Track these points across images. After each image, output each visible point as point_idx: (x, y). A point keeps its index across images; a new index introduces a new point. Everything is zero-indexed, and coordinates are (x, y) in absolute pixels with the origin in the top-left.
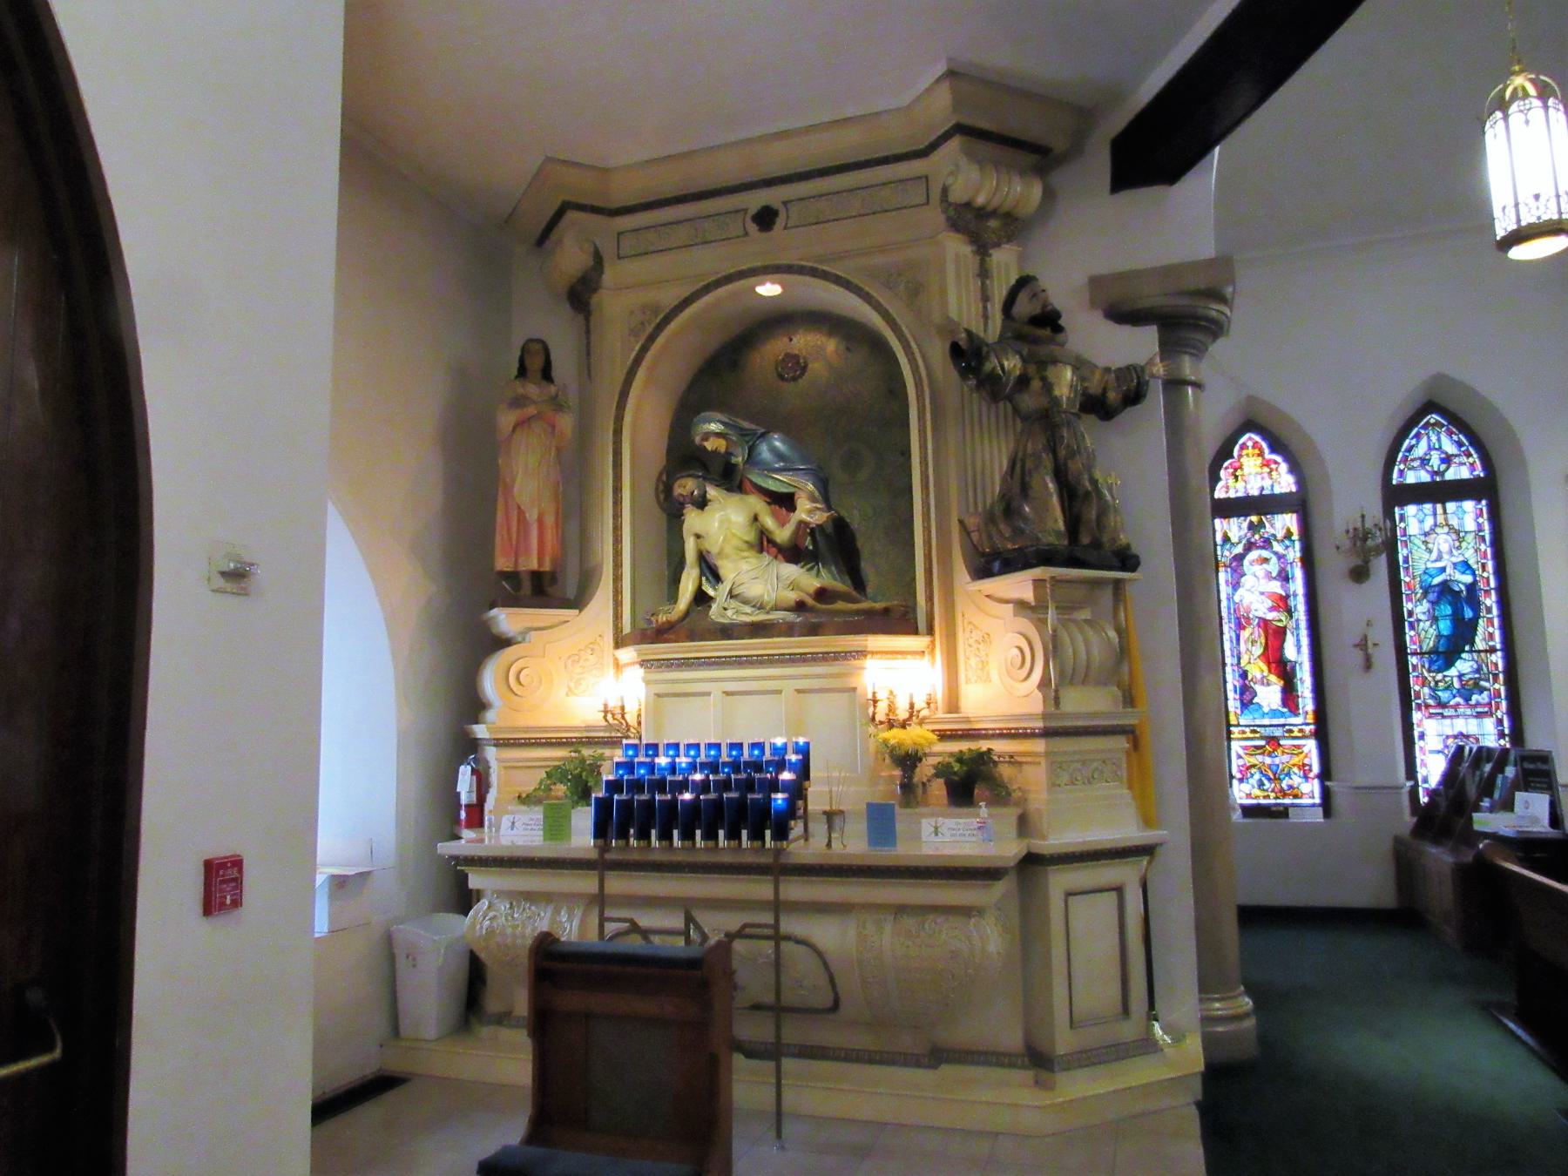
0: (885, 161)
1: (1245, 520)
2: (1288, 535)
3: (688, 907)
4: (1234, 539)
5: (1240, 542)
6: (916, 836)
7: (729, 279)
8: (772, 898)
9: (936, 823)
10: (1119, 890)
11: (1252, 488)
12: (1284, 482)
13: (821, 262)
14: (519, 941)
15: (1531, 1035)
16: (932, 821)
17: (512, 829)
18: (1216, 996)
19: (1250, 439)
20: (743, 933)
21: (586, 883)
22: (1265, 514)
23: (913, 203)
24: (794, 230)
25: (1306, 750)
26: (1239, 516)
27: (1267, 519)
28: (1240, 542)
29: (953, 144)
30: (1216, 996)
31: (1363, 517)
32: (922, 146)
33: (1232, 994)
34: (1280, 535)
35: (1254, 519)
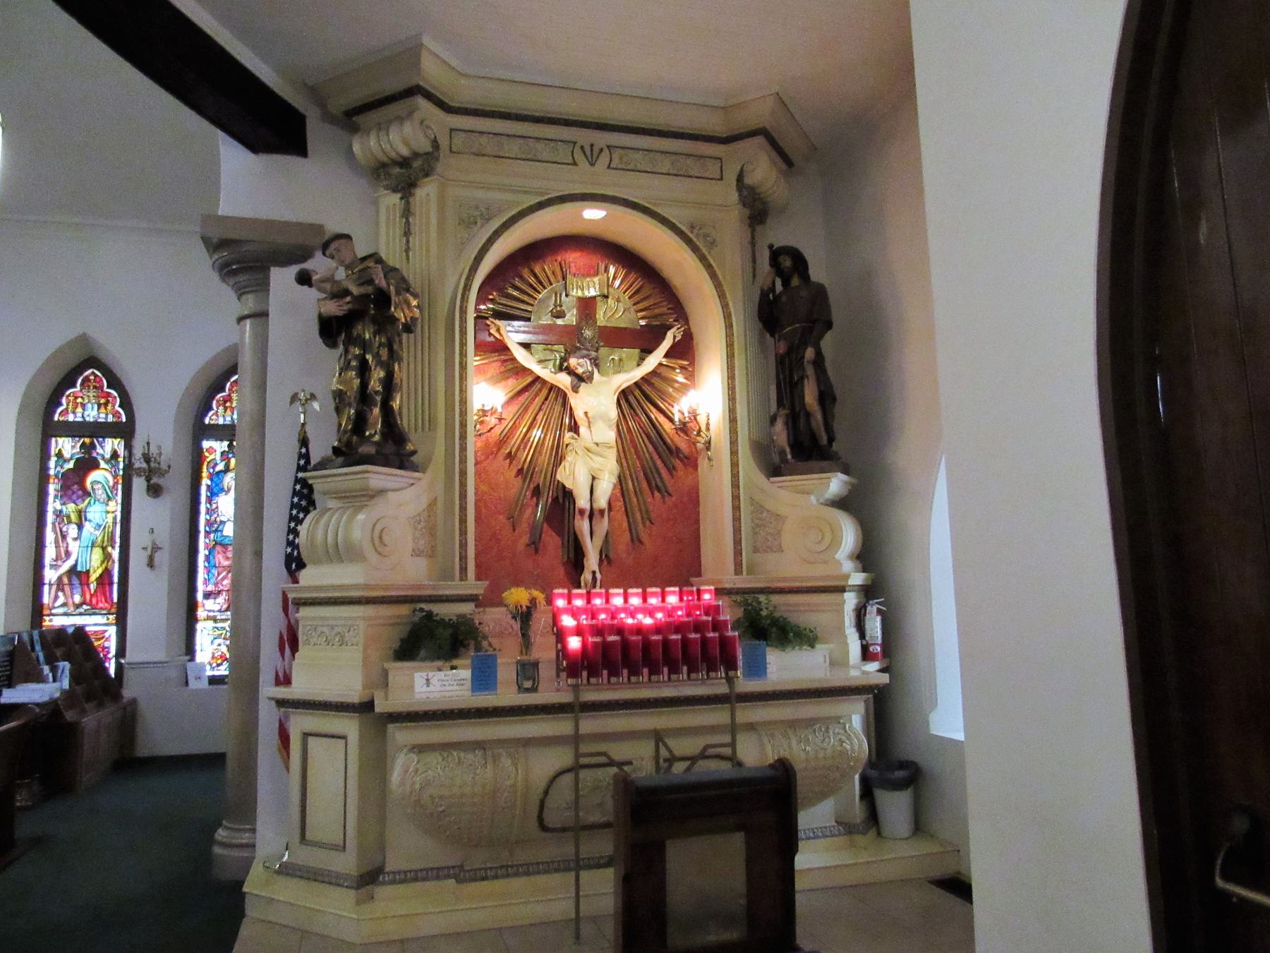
0: (568, 123)
1: (79, 441)
2: (115, 455)
3: (658, 737)
4: (67, 455)
5: (71, 459)
6: (411, 687)
7: (562, 199)
8: (572, 732)
9: (427, 675)
10: (306, 735)
11: (88, 415)
12: (112, 413)
13: (655, 204)
14: (467, 790)
15: (860, 790)
16: (424, 674)
17: (428, 686)
18: (247, 827)
19: (93, 373)
20: (706, 754)
21: (560, 726)
22: (97, 437)
23: (660, 171)
24: (614, 171)
25: (107, 635)
26: (73, 436)
27: (98, 441)
28: (71, 459)
29: (757, 141)
30: (247, 827)
31: (148, 444)
32: (453, 104)
33: (237, 826)
34: (108, 456)
35: (87, 440)
